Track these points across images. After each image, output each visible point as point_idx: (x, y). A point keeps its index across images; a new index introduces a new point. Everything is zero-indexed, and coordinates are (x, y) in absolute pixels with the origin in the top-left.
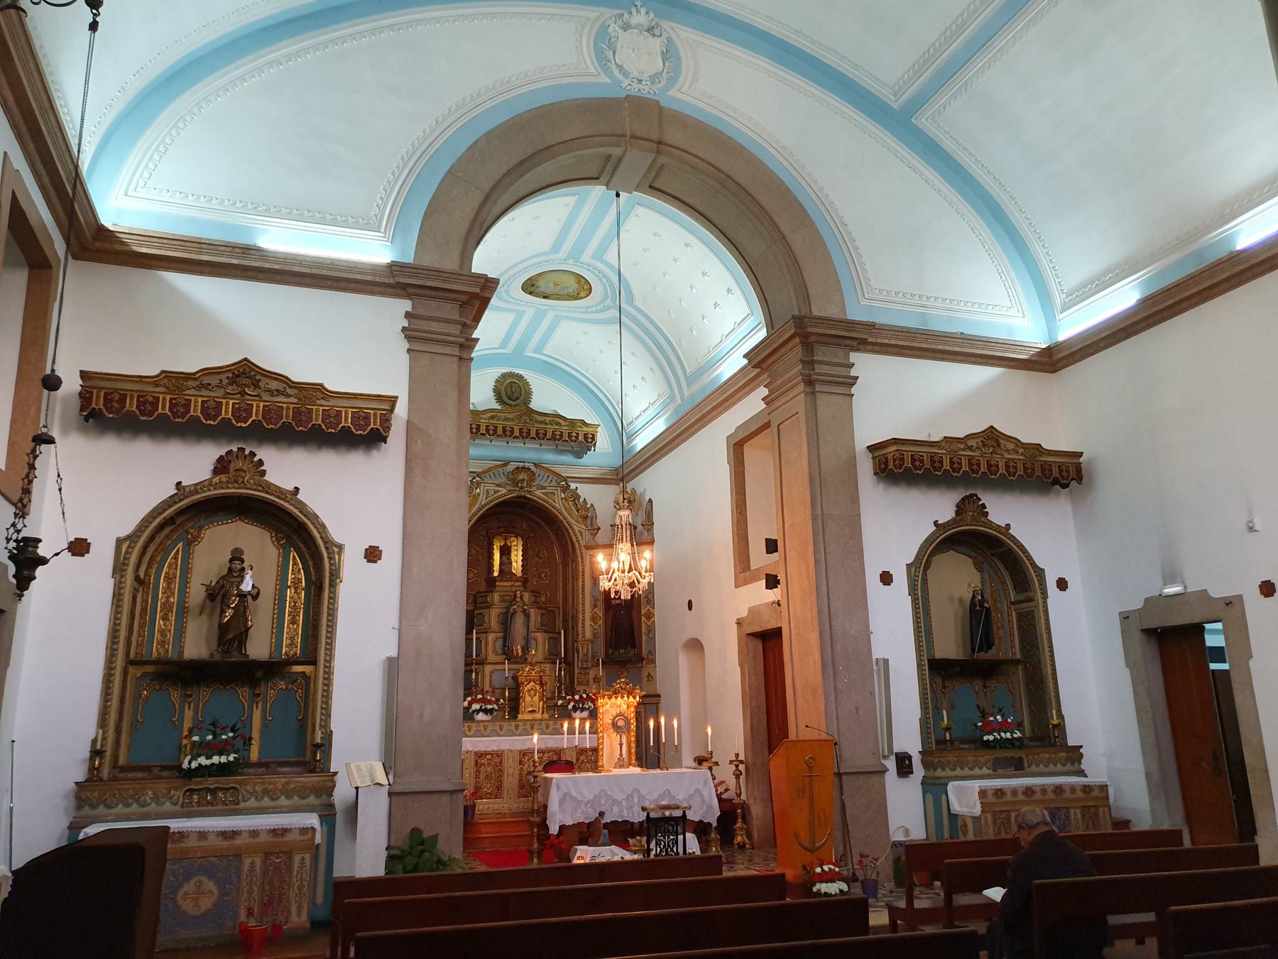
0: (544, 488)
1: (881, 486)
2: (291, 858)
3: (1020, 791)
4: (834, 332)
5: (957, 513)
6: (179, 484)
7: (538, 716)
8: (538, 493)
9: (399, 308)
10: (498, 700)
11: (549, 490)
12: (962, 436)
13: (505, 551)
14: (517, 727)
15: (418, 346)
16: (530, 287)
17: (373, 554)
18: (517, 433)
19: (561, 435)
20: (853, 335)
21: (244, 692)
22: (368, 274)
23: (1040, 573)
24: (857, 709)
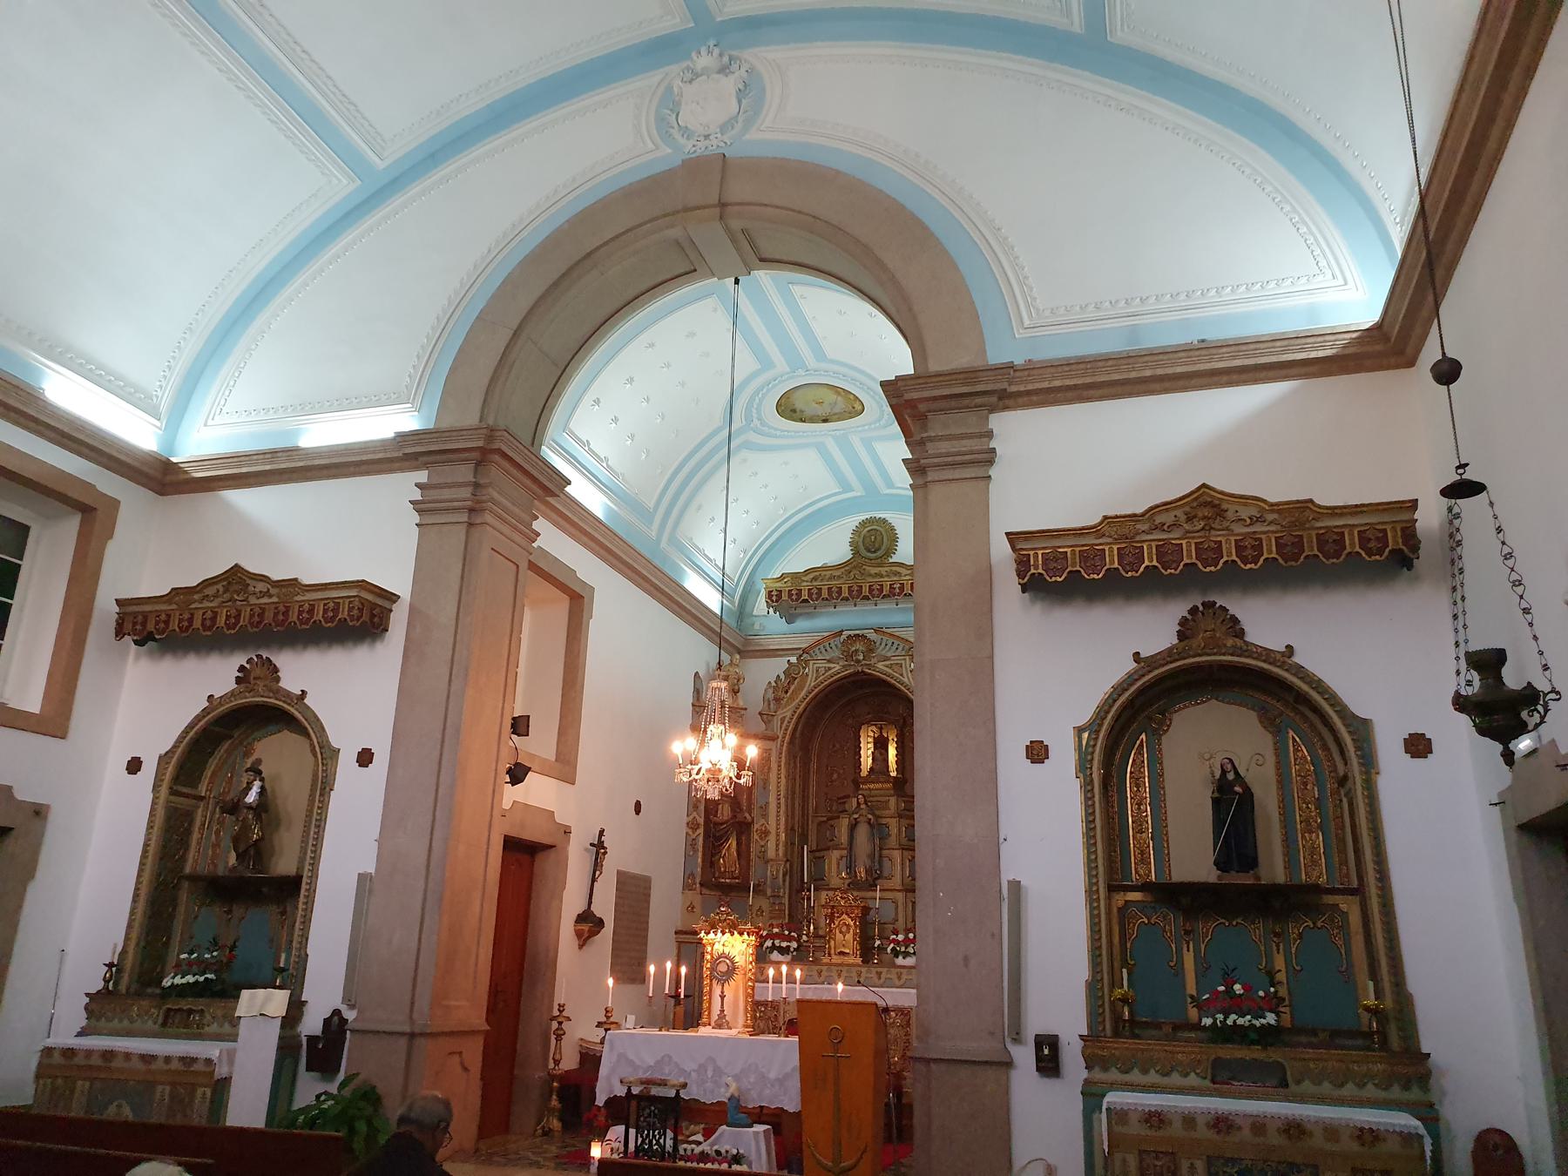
0: (887, 659)
1: (1038, 608)
2: (193, 1091)
3: (1201, 1121)
4: (946, 392)
5: (1182, 636)
6: (211, 697)
7: (851, 960)
8: (880, 665)
9: (405, 485)
10: (800, 936)
11: (895, 660)
12: (1139, 511)
13: (881, 745)
14: (820, 974)
15: (429, 519)
16: (788, 408)
17: (365, 758)
18: (845, 594)
19: (902, 587)
20: (979, 388)
21: (1257, 930)
22: (354, 454)
23: (1362, 729)
24: (966, 959)
